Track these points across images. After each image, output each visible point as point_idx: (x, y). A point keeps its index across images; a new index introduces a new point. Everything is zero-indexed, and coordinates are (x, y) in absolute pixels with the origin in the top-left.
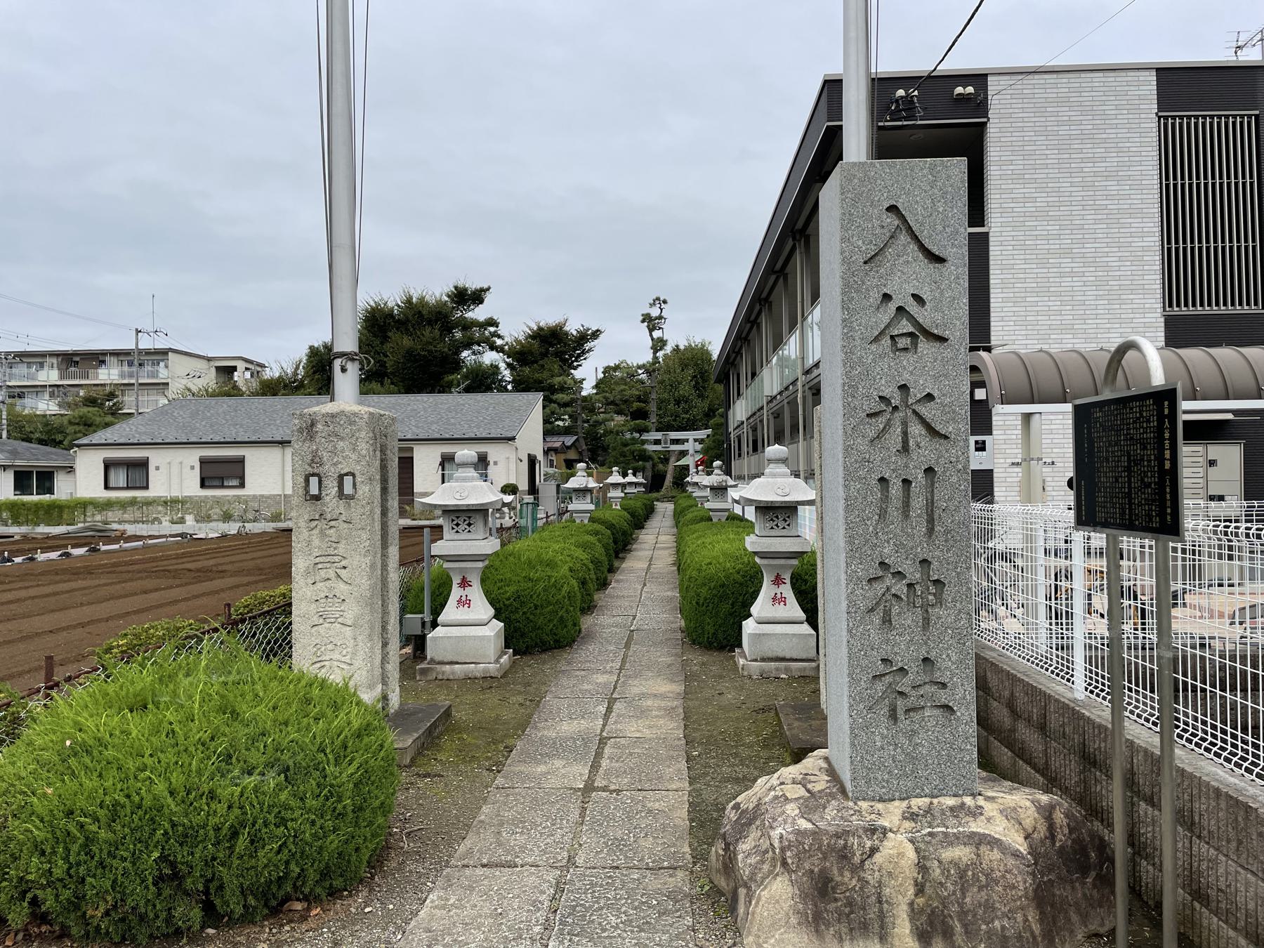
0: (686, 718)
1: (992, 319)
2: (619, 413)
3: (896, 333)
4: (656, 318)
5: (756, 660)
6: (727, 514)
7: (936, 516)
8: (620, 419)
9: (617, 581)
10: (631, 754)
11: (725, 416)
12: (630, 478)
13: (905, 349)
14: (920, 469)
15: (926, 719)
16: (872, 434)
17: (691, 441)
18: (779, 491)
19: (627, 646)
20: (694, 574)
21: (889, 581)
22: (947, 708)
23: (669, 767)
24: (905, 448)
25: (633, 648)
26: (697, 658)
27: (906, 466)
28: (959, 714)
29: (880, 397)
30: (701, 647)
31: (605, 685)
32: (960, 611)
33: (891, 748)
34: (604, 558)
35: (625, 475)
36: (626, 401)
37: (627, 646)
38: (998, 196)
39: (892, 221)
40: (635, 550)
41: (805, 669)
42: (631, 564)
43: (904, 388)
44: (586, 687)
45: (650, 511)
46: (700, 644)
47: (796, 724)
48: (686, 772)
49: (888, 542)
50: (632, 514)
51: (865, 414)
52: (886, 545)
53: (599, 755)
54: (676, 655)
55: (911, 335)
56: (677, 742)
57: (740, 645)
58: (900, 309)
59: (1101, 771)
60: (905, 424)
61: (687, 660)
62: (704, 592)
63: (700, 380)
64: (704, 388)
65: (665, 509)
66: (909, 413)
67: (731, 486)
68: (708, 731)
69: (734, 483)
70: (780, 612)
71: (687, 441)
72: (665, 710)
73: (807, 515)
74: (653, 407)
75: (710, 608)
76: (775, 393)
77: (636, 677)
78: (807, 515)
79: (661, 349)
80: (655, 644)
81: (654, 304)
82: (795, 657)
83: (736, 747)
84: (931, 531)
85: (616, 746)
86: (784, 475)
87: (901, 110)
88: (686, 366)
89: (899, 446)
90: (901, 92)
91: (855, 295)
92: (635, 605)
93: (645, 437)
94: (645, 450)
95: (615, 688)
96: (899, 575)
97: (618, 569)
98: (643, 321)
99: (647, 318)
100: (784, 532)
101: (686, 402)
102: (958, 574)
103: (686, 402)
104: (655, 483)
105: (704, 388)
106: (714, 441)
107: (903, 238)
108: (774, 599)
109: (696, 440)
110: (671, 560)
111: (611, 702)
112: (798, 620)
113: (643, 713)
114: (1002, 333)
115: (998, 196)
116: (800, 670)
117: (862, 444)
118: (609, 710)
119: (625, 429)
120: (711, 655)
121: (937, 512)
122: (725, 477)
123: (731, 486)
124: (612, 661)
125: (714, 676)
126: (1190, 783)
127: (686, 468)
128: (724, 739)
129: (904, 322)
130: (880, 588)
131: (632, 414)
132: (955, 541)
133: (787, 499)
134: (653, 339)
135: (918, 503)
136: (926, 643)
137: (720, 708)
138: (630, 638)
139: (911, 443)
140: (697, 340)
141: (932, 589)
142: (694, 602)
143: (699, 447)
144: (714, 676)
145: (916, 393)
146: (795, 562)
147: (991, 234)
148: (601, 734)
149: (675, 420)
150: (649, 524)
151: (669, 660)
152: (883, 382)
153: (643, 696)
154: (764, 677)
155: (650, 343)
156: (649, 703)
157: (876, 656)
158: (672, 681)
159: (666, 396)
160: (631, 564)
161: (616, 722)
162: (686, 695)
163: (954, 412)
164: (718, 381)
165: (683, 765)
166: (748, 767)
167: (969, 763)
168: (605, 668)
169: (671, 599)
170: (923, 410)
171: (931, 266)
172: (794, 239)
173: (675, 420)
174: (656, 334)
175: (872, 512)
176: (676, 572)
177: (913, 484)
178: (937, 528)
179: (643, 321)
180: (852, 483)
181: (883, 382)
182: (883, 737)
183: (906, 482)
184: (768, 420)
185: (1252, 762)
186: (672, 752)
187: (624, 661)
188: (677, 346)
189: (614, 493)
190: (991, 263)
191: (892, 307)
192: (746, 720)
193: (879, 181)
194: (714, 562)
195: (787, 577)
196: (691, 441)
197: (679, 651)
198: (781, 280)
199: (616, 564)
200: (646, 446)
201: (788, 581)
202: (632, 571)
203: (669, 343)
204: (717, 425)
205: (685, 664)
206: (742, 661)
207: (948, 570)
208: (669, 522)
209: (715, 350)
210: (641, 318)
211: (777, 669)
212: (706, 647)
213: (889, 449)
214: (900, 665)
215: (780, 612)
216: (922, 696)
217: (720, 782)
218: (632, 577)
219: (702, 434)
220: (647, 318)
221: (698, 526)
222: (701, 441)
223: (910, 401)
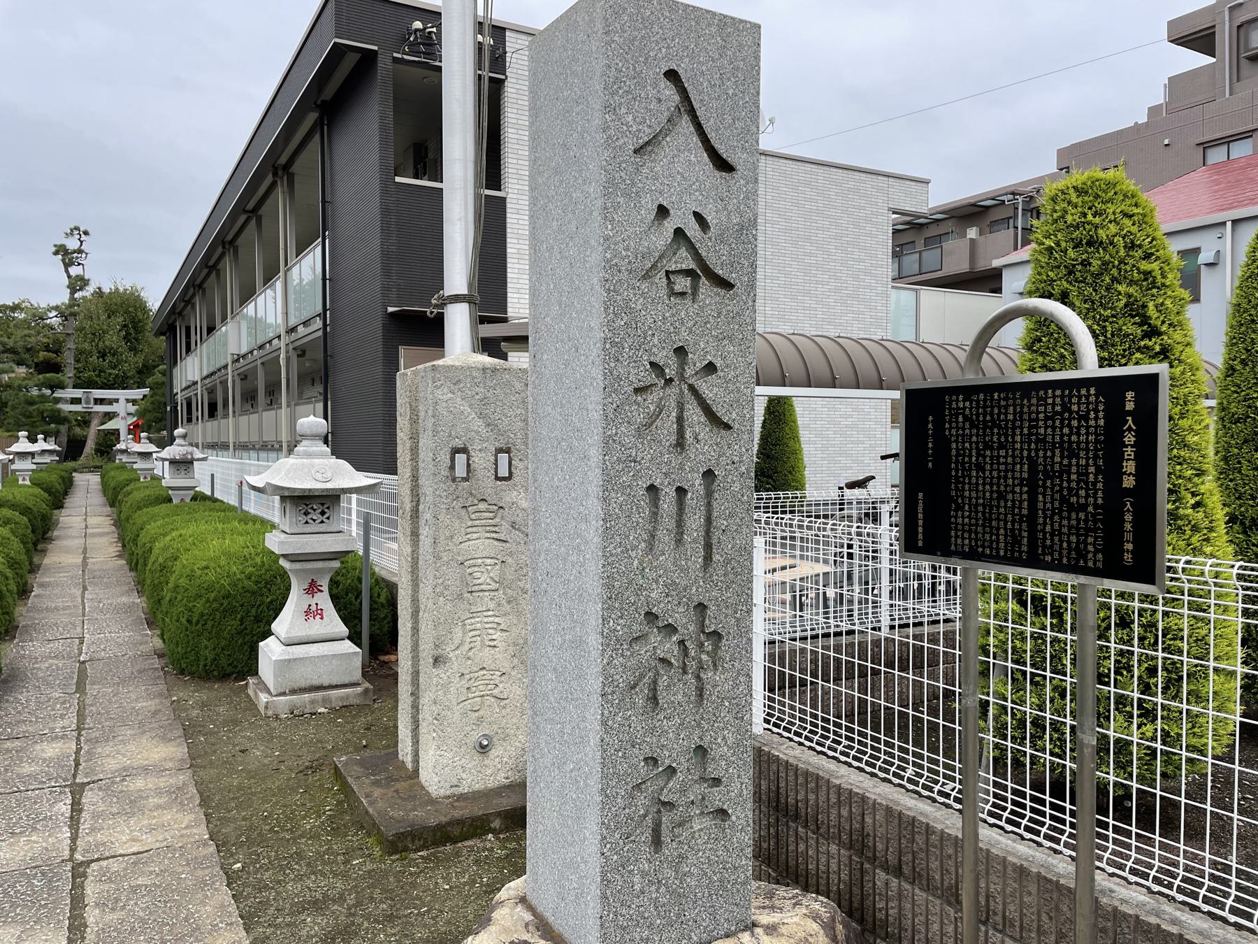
0: (205, 802)
1: (509, 290)
2: (19, 364)
3: (673, 268)
4: (74, 252)
5: (284, 694)
6: (192, 492)
7: (714, 541)
8: (22, 371)
9: (42, 585)
10: (134, 890)
11: (169, 374)
12: (41, 445)
13: (683, 294)
14: (698, 472)
15: (697, 835)
16: (640, 419)
17: (122, 401)
18: (319, 476)
19: (81, 687)
20: (183, 582)
21: (655, 638)
22: (722, 813)
23: (203, 903)
24: (680, 444)
25: (92, 690)
26: (193, 696)
27: (681, 468)
28: (734, 818)
29: (651, 363)
30: (193, 678)
31: (59, 761)
32: (739, 674)
33: (653, 888)
34: (24, 557)
35: (33, 439)
36: (28, 350)
37: (81, 687)
38: (515, 161)
39: (669, 92)
40: (58, 538)
41: (348, 696)
42: (56, 559)
43: (681, 352)
44: (27, 769)
45: (68, 485)
46: (192, 674)
47: (377, 792)
48: (233, 908)
49: (657, 582)
50: (48, 490)
51: (631, 388)
52: (654, 586)
53: (78, 901)
54: (160, 695)
55: (689, 273)
56: (204, 851)
57: (254, 672)
58: (679, 232)
59: (806, 827)
60: (681, 407)
61: (178, 701)
62: (199, 605)
63: (132, 331)
64: (137, 340)
65: (88, 483)
66: (685, 388)
67: (198, 460)
68: (244, 819)
69: (201, 456)
70: (316, 628)
71: (117, 401)
72: (169, 793)
73: (354, 506)
74: (68, 358)
75: (209, 626)
76: (244, 350)
77: (107, 740)
78: (354, 506)
79: (81, 289)
80: (123, 681)
81: (72, 234)
82: (334, 683)
83: (294, 839)
84: (708, 558)
85: (105, 876)
86: (322, 455)
87: (420, 44)
88: (113, 313)
89: (673, 439)
90: (418, 25)
91: (621, 200)
92: (78, 623)
93: (59, 394)
94: (59, 411)
95: (77, 764)
96: (671, 629)
97: (39, 567)
98: (56, 253)
99: (61, 250)
100: (323, 528)
101: (114, 355)
102: (738, 620)
103: (114, 355)
104: (73, 449)
105: (137, 340)
106: (152, 403)
107: (686, 125)
108: (307, 612)
109: (128, 401)
110: (114, 549)
111: (77, 791)
112: (338, 636)
113: (133, 805)
114: (518, 306)
115: (515, 161)
116: (342, 699)
117: (626, 434)
118: (76, 808)
119: (31, 383)
120: (211, 689)
121: (716, 535)
122: (190, 449)
123: (198, 460)
124: (62, 717)
125: (225, 723)
126: (988, 861)
127: (116, 433)
128: (271, 830)
129: (683, 252)
130: (643, 651)
131: (37, 365)
132: (736, 574)
133: (329, 486)
134: (69, 276)
135: (695, 522)
136: (699, 725)
137: (251, 775)
138: (82, 675)
139: (688, 434)
140: (125, 283)
141: (708, 646)
142: (184, 620)
143: (132, 408)
144: (225, 723)
145: (696, 361)
146: (336, 564)
147: (508, 200)
148: (71, 859)
149: (99, 376)
150: (69, 502)
151: (152, 704)
152: (656, 340)
153: (126, 773)
154: (297, 715)
155: (66, 281)
156: (139, 783)
157: (637, 755)
158: (165, 739)
159: (87, 346)
160: (56, 559)
161: (93, 829)
162: (195, 760)
163: (739, 391)
164: (160, 333)
165: (224, 894)
166: (323, 875)
167: (744, 884)
168: (52, 730)
169: (129, 608)
170: (708, 388)
171: (717, 174)
172: (275, 174)
173: (99, 376)
174: (74, 271)
175: (637, 537)
176: (127, 567)
177: (690, 494)
178: (716, 557)
179: (56, 253)
180: (613, 495)
181: (656, 340)
182: (644, 874)
183: (681, 491)
184: (234, 382)
185: (1136, 859)
186: (200, 873)
187: (81, 716)
188: (99, 288)
189: (19, 465)
190: (508, 230)
191: (669, 226)
192: (294, 790)
193: (656, 28)
194: (212, 565)
195: (324, 584)
196: (122, 401)
197: (162, 687)
198: (253, 222)
199: (36, 560)
200: (60, 406)
201: (325, 588)
202: (60, 568)
203: (92, 283)
204: (157, 383)
205: (177, 707)
206: (264, 698)
207: (727, 616)
208: (97, 499)
209: (154, 297)
210: (54, 249)
211: (312, 702)
212: (200, 678)
213: (660, 442)
214: (667, 762)
215: (316, 628)
216: (692, 803)
217: (292, 914)
218: (62, 577)
219: (137, 393)
220: (61, 250)
221: (156, 509)
222: (134, 402)
223: (689, 372)
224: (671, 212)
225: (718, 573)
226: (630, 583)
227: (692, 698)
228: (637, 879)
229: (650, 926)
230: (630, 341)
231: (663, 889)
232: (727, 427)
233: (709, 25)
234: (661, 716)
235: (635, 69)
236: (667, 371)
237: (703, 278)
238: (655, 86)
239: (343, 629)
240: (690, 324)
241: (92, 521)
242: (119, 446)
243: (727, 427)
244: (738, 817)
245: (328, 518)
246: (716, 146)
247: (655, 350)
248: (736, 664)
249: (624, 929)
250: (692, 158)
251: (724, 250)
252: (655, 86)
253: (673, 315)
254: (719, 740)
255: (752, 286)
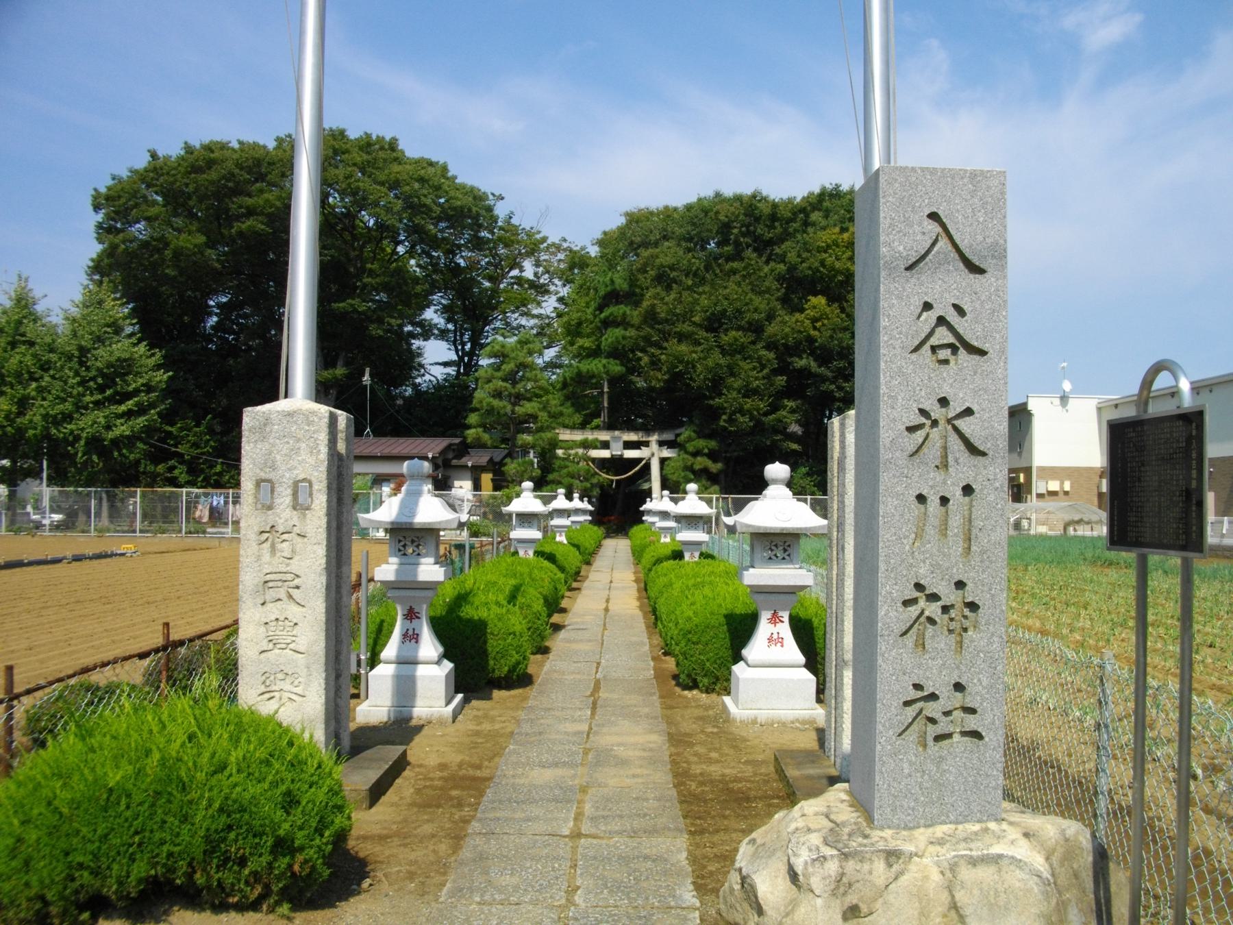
3: (937, 343)
14: (958, 486)
27: (945, 483)
33: (918, 775)
39: (934, 228)
49: (924, 562)
51: (904, 427)
52: (922, 565)
56: (670, 792)
91: (895, 302)
102: (993, 596)
130: (914, 611)
132: (991, 562)
136: (958, 668)
139: (950, 459)
171: (972, 276)
178: (974, 548)
180: (890, 499)
181: (923, 393)
182: (911, 763)
183: (944, 501)
207: (982, 592)
213: (927, 464)
224: (935, 305)
225: (975, 560)
226: (903, 561)
227: (953, 648)
228: (906, 765)
229: (916, 800)
230: (903, 395)
231: (926, 777)
232: (984, 454)
233: (962, 178)
234: (927, 656)
235: (904, 216)
236: (932, 414)
237: (961, 349)
238: (920, 224)
239: (801, 659)
240: (951, 381)
241: (617, 575)
242: (648, 506)
243: (984, 454)
244: (991, 740)
245: (789, 555)
246: (970, 258)
247: (922, 400)
248: (991, 628)
249: (895, 797)
250: (951, 268)
251: (979, 328)
252: (920, 224)
253: (937, 376)
254: (975, 681)
255: (1003, 351)
